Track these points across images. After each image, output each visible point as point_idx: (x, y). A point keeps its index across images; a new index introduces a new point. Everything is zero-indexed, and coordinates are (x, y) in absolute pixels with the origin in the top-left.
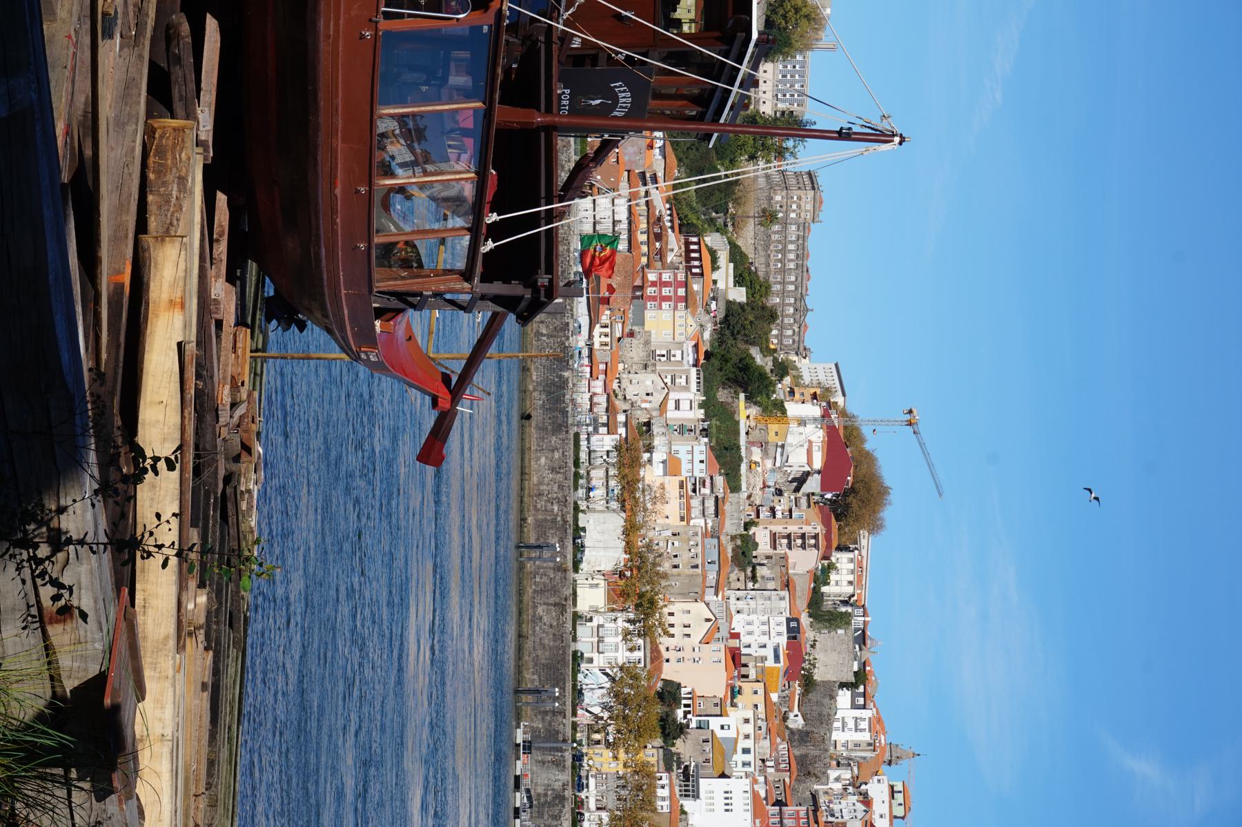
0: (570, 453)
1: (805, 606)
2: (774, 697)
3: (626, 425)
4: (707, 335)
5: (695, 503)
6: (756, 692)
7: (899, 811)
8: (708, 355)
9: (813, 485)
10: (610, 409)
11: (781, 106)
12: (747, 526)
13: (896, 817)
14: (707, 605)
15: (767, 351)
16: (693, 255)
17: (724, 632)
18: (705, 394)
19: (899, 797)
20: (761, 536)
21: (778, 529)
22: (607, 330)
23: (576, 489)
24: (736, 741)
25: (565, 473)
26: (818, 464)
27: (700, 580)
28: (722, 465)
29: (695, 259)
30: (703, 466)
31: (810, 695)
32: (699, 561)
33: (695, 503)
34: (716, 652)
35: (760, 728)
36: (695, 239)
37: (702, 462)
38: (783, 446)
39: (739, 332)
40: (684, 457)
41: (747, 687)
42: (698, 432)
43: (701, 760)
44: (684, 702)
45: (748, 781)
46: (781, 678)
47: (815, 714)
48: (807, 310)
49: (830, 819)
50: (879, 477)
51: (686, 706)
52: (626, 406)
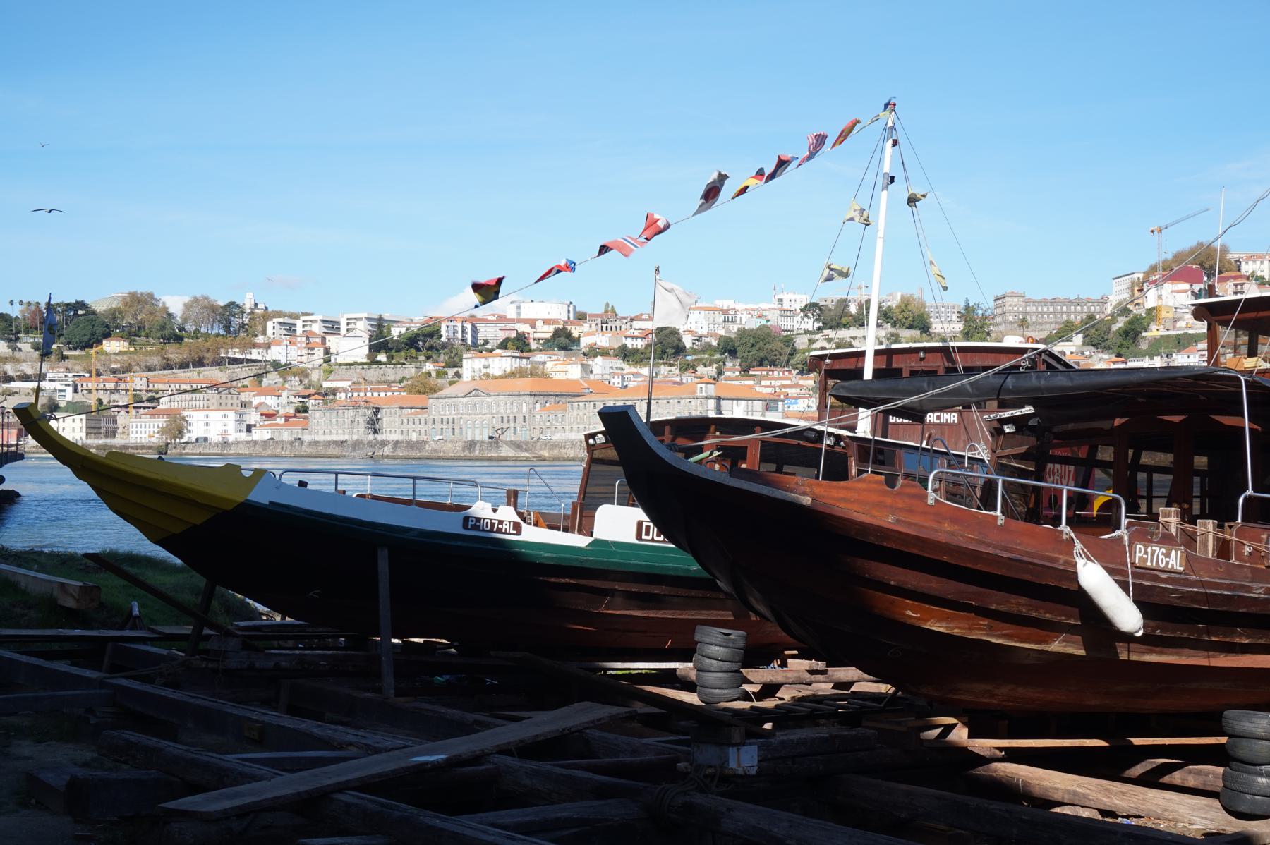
4: (1106, 357)
8: (1119, 355)
11: (955, 317)
15: (1114, 320)
18: (1144, 356)
23: (836, 397)
26: (1186, 286)
28: (1189, 344)
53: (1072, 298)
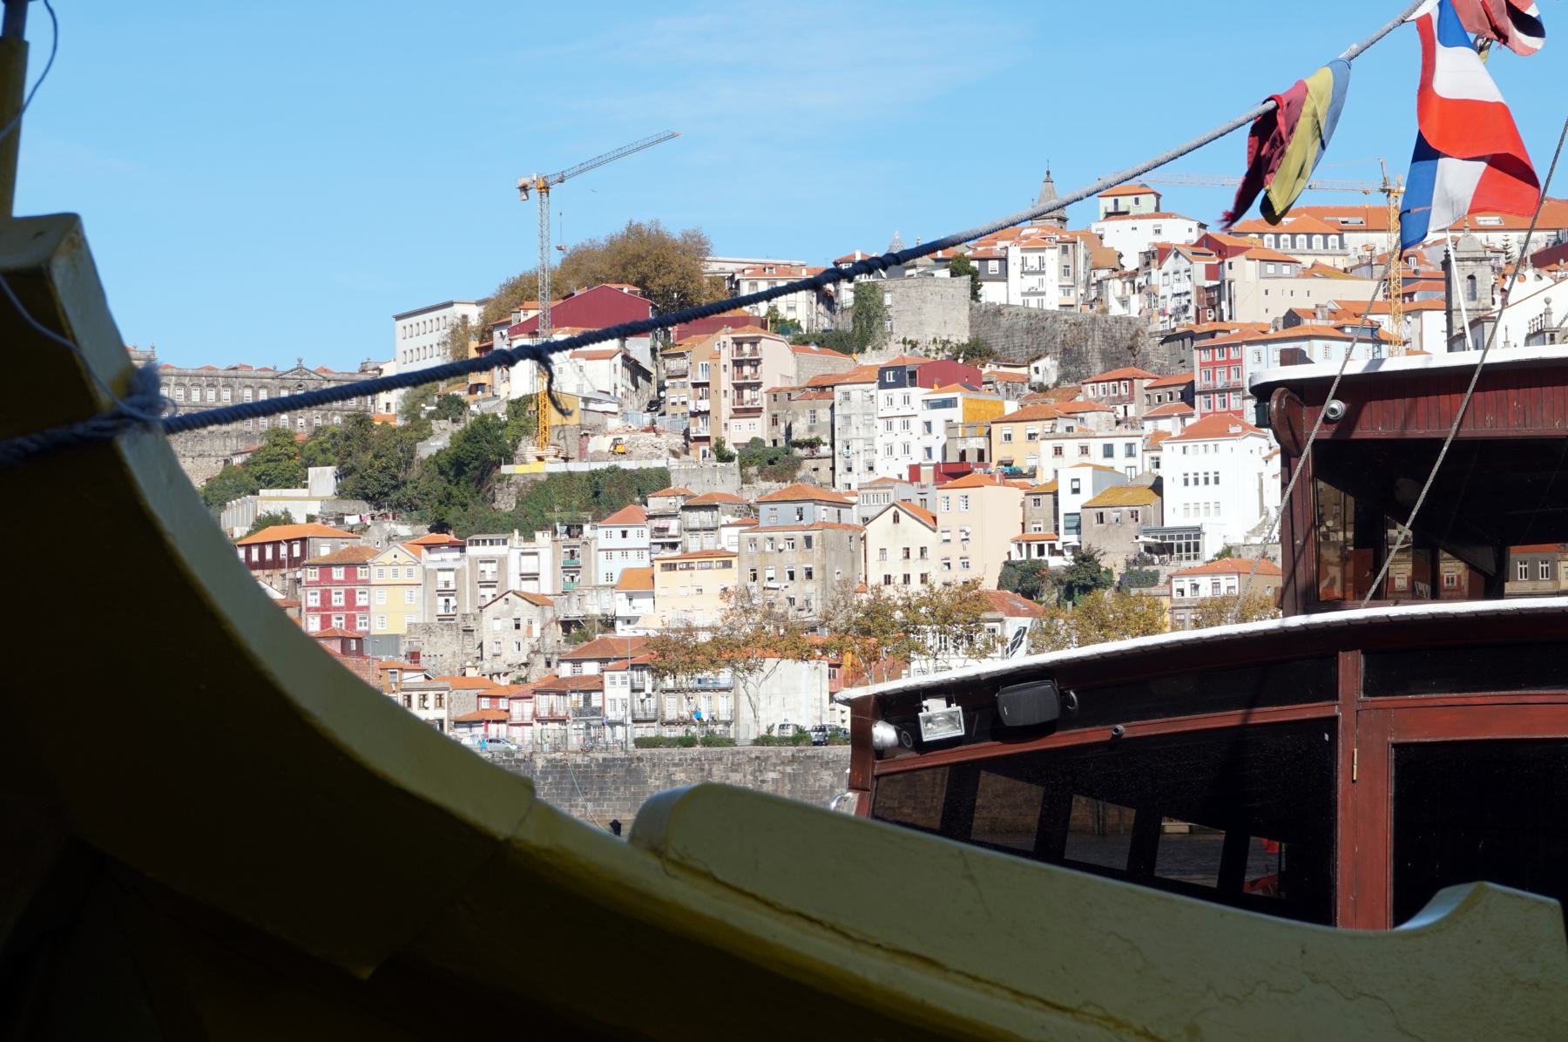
0: (676, 752)
1: (848, 359)
2: (1011, 407)
3: (577, 662)
4: (404, 530)
5: (694, 544)
6: (1008, 437)
7: (1148, 203)
8: (440, 527)
9: (640, 347)
10: (558, 688)
12: (725, 457)
13: (1157, 209)
14: (866, 520)
16: (269, 555)
17: (911, 492)
18: (508, 529)
19: (1126, 203)
20: (739, 433)
21: (727, 405)
22: (415, 696)
24: (1096, 468)
25: (711, 762)
27: (830, 532)
29: (276, 552)
30: (631, 532)
31: (995, 348)
32: (799, 536)
33: (694, 544)
34: (948, 502)
35: (1069, 429)
36: (241, 553)
37: (624, 534)
38: (586, 400)
39: (394, 477)
40: (617, 565)
41: (1000, 452)
42: (574, 542)
43: (1132, 526)
44: (1034, 555)
45: (1166, 447)
46: (981, 397)
47: (1028, 340)
48: (300, 368)
49: (1192, 312)
50: (612, 242)
51: (1041, 551)
52: (540, 662)
53: (281, 369)
